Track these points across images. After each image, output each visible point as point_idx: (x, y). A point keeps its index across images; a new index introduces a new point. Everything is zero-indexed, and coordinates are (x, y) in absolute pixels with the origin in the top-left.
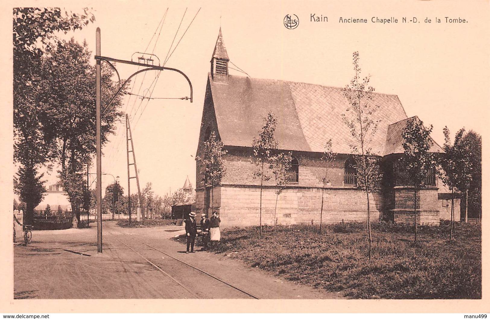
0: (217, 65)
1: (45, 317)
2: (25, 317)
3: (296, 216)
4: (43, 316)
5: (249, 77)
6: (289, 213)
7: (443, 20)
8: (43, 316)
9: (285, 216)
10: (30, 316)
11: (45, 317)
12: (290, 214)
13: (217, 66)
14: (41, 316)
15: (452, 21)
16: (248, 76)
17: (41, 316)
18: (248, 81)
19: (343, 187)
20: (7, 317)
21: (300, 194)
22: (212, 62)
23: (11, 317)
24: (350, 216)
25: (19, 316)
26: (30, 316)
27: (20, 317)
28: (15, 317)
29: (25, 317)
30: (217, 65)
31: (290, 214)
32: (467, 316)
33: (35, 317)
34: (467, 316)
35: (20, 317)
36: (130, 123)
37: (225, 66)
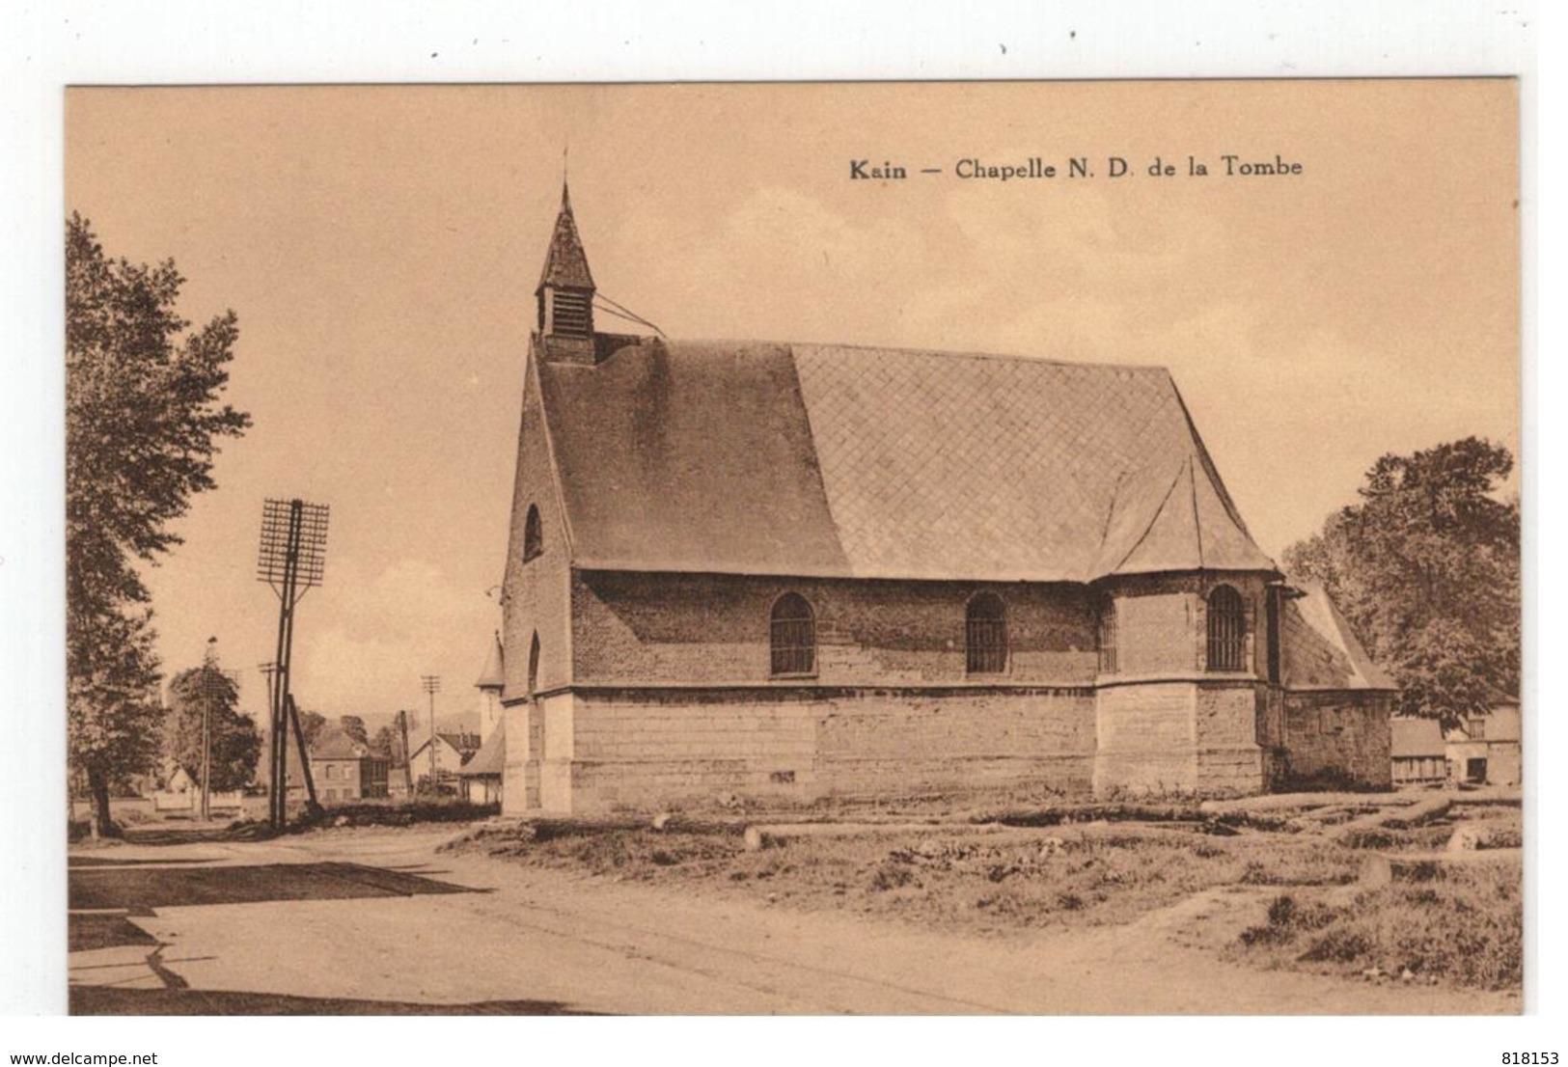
0: (558, 306)
1: (145, 1060)
2: (79, 1060)
3: (810, 778)
4: (137, 1059)
5: (660, 337)
6: (789, 768)
7: (1217, 170)
8: (137, 1059)
9: (777, 778)
10: (98, 1059)
11: (145, 1060)
12: (792, 774)
13: (555, 309)
14: (130, 1059)
15: (1246, 170)
16: (658, 334)
17: (130, 1059)
18: (658, 354)
19: (962, 683)
20: (35, 1060)
21: (823, 709)
22: (540, 293)
23: (22, 1061)
24: (986, 772)
25: (60, 1059)
26: (98, 1059)
27: (64, 1060)
28: (48, 1060)
29: (79, 1060)
30: (558, 306)
31: (792, 774)
32: (103, 1059)
33: (113, 1060)
34: (103, 1059)
35: (64, 1060)
36: (267, 701)
37: (582, 309)
